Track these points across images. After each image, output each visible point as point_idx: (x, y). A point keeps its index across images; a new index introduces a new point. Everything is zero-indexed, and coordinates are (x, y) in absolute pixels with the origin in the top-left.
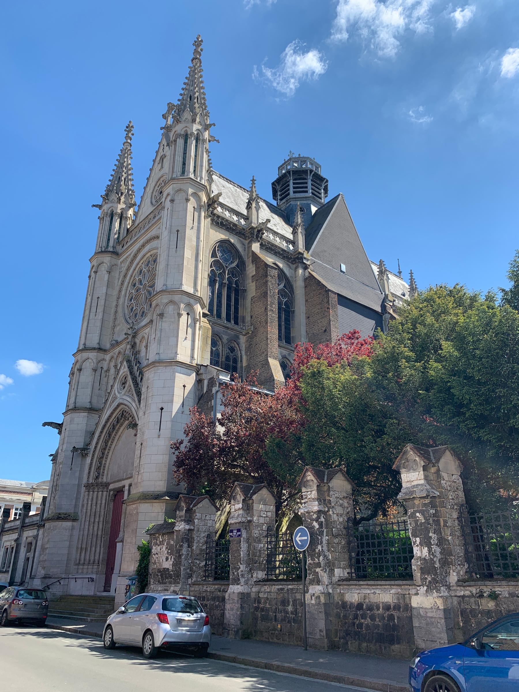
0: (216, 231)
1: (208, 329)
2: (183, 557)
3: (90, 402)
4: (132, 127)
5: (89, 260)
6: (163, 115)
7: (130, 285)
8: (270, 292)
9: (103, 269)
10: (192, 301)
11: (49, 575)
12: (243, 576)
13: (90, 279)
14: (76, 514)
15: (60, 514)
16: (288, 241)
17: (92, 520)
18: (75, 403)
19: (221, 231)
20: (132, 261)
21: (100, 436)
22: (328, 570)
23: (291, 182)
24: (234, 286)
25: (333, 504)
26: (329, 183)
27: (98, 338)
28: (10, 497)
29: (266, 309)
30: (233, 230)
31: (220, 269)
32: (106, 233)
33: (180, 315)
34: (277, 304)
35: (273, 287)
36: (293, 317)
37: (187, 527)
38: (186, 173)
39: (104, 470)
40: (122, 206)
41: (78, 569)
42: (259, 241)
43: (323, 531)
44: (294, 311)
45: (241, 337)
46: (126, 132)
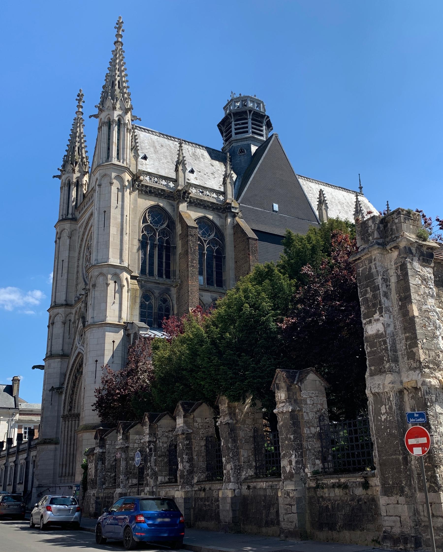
0: (146, 200)
1: (136, 290)
3: (62, 350)
4: (82, 95)
7: (86, 247)
8: (191, 250)
9: (65, 235)
10: (118, 271)
11: (41, 485)
12: (122, 482)
13: (56, 244)
14: (57, 438)
15: (45, 439)
16: (218, 193)
17: (69, 443)
18: (51, 351)
19: (150, 198)
20: (86, 227)
21: (69, 378)
23: (233, 123)
24: (165, 245)
25: (159, 436)
26: (270, 118)
29: (188, 265)
30: (162, 195)
31: (151, 232)
32: (66, 201)
33: (108, 285)
36: (224, 262)
37: (101, 451)
38: (110, 158)
39: (75, 403)
40: (77, 174)
41: (61, 480)
42: (186, 201)
44: (225, 257)
45: (172, 289)
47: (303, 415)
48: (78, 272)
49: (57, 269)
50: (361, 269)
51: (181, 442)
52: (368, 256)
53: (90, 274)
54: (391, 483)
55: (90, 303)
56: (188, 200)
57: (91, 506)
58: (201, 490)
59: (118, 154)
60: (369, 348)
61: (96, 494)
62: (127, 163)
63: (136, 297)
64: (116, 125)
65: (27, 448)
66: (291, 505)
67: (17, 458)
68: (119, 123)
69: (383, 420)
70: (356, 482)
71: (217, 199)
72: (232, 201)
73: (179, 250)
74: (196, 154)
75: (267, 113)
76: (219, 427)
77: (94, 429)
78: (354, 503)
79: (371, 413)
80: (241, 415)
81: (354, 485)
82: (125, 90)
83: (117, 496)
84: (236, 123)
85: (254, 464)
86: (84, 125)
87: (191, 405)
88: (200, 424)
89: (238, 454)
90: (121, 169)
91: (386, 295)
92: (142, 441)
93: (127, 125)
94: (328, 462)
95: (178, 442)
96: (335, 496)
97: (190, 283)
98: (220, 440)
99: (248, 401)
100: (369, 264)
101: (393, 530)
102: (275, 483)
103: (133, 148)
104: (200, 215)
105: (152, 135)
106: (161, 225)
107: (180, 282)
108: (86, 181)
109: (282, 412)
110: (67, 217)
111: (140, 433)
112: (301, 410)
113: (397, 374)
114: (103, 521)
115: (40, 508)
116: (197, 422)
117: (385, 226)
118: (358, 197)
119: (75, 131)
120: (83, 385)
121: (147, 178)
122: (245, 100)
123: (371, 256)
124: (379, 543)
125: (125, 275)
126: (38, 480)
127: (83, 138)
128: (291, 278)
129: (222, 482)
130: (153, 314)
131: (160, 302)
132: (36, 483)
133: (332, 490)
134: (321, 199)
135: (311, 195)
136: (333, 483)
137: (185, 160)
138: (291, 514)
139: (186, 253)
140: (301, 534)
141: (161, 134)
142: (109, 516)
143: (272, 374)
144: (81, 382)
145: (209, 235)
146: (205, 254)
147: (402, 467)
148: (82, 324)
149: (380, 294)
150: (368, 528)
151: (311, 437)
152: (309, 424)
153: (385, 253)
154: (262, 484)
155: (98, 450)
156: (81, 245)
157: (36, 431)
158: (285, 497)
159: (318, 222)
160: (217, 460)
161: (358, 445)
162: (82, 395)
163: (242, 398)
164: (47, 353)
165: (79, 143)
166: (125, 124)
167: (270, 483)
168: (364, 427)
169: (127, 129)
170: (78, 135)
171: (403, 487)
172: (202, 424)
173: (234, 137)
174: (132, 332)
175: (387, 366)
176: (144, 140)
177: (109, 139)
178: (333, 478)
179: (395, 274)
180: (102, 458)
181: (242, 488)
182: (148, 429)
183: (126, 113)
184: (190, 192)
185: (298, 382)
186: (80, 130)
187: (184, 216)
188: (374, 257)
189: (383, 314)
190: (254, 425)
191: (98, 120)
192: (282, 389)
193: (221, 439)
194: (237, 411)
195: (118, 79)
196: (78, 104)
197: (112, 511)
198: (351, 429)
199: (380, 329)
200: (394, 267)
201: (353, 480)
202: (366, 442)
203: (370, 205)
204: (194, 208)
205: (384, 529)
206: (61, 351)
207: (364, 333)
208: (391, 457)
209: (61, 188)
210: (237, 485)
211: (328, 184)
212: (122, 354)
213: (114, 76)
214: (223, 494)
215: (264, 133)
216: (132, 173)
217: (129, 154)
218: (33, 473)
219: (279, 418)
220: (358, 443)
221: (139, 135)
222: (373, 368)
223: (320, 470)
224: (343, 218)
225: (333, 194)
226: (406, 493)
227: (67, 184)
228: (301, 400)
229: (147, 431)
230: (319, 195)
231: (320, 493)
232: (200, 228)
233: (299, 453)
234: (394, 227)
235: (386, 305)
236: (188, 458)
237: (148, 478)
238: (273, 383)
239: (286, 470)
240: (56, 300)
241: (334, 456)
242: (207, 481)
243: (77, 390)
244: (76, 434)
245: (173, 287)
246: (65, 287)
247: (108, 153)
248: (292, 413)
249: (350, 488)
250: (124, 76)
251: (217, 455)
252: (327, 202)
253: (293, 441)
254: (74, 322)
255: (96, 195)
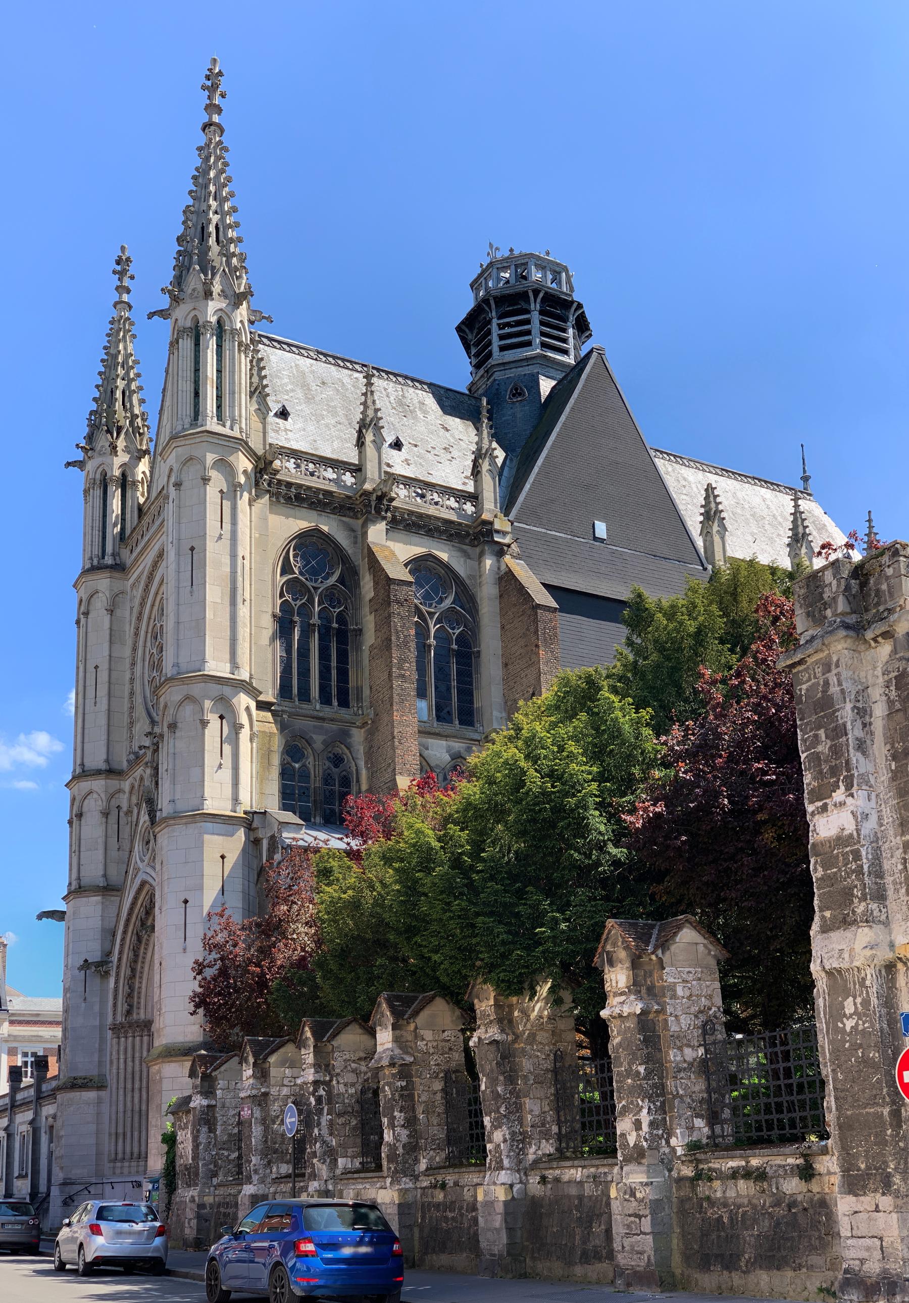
0: (287, 517)
1: (271, 734)
2: (201, 1147)
3: (105, 875)
4: (128, 260)
5: (74, 586)
6: (178, 239)
7: (149, 635)
8: (398, 638)
10: (227, 690)
11: (70, 1179)
12: (256, 1171)
13: (79, 627)
14: (102, 1076)
15: (75, 1079)
16: (462, 496)
17: (129, 1086)
18: (79, 878)
20: (147, 586)
21: (123, 939)
22: (328, 1160)
23: (495, 322)
24: (335, 625)
25: (337, 1071)
27: (104, 750)
28: (52, 1034)
29: (390, 674)
30: (325, 504)
31: (302, 595)
32: (98, 524)
33: (204, 723)
34: (414, 660)
35: (403, 626)
36: (478, 665)
37: (205, 1102)
38: (200, 418)
39: (139, 998)
40: (122, 458)
41: (114, 1168)
42: (384, 518)
43: (322, 1109)
44: (479, 652)
46: (117, 276)
47: (666, 1021)
48: (132, 693)
49: (85, 687)
50: (804, 687)
51: (389, 1084)
52: (821, 655)
53: (162, 699)
54: (863, 1166)
55: (165, 767)
56: (389, 514)
57: (187, 1225)
58: (435, 1187)
59: (219, 407)
60: (820, 869)
61: (197, 1199)
62: (241, 428)
63: (270, 751)
64: (212, 335)
65: (34, 1099)
66: (640, 1217)
67: (11, 1121)
68: (220, 330)
69: (848, 1029)
70: (784, 1166)
71: (459, 511)
72: (496, 516)
73: (370, 638)
74: (408, 401)
75: (576, 297)
76: (476, 1050)
77: (186, 1055)
78: (781, 1211)
79: (822, 1015)
80: (526, 1024)
81: (781, 1172)
82: (232, 248)
83: (247, 1201)
84: (502, 321)
85: (555, 1129)
86: (134, 336)
87: (407, 1002)
88: (430, 1045)
89: (519, 1107)
90: (227, 444)
91: (861, 746)
92: (299, 1081)
93: (239, 334)
94: (722, 1122)
95: (382, 1083)
96: (739, 1195)
97: (396, 716)
98: (475, 1078)
99: (544, 989)
100: (823, 674)
101: (866, 1267)
102: (602, 1170)
103: (256, 389)
104: (417, 550)
105: (298, 357)
106: (326, 578)
107: (372, 716)
108: (144, 473)
109: (620, 1016)
110: (101, 561)
111: (295, 1064)
112: (662, 1009)
113: (882, 926)
114: (221, 1255)
115: (74, 1228)
116: (423, 1039)
117: (863, 585)
118: (800, 502)
119: (112, 351)
120: (156, 956)
121: (291, 464)
122: (523, 264)
123: (829, 655)
124: (834, 1295)
125: (244, 701)
126: (62, 1168)
127: (132, 368)
128: (639, 706)
129: (482, 1168)
130: (312, 791)
131: (327, 763)
132: (58, 1176)
133: (731, 1183)
134: (710, 509)
135: (684, 497)
136: (732, 1168)
137: (381, 418)
138: (638, 1235)
139: (386, 645)
140: (661, 1277)
141: (322, 354)
142: (234, 1243)
143: (596, 933)
144: (150, 949)
145: (441, 600)
146: (430, 646)
147: (889, 1132)
148: (147, 817)
149: (848, 745)
150: (809, 1263)
151: (685, 1069)
152: (680, 1041)
153: (862, 647)
154: (573, 1171)
155: (198, 1102)
156: (137, 629)
157: (52, 1061)
158: (626, 1200)
159: (703, 565)
160: (471, 1123)
161: (792, 1084)
162: (157, 978)
163: (526, 985)
164: (70, 884)
165: (123, 379)
166: (235, 332)
167: (592, 1170)
168: (805, 1045)
169: (240, 344)
170: (120, 359)
171: (889, 1175)
172: (435, 1044)
173: (497, 356)
174: (264, 835)
175: (861, 908)
176: (279, 371)
177: (197, 370)
178: (732, 1158)
179: (884, 698)
180: (207, 1118)
181: (527, 1180)
182: (311, 1055)
183: (237, 305)
184: (393, 495)
185: (656, 948)
186: (125, 348)
187: (380, 557)
188: (835, 659)
189: (854, 790)
190: (554, 1044)
191: (169, 323)
192: (620, 965)
193: (481, 1075)
194: (516, 1014)
195: (215, 219)
196: (119, 283)
197: (241, 1232)
198: (775, 1050)
199: (846, 826)
200: (881, 680)
201: (779, 1161)
202: (809, 1079)
203: (827, 520)
204: (402, 535)
205: (845, 1266)
206: (102, 879)
207: (810, 834)
208: (864, 1111)
209: (86, 492)
210: (518, 1176)
211: (727, 471)
212: (243, 885)
213: (205, 212)
214: (486, 1194)
215: (571, 346)
216: (255, 454)
217: (245, 406)
218: (51, 1154)
219: (614, 1030)
220: (790, 1081)
221: (268, 357)
222: (828, 914)
223: (704, 1141)
224: (764, 560)
225: (739, 494)
226: (895, 1187)
227: (98, 482)
228: (663, 987)
229: (310, 1059)
230: (705, 499)
231: (704, 1191)
232: (419, 583)
233: (658, 1104)
234: (884, 587)
235: (862, 770)
236: (405, 1118)
237: (315, 1161)
238: (600, 950)
239: (627, 1142)
240: (85, 761)
241: (735, 1110)
242: (449, 1167)
243: (142, 968)
244: (144, 1065)
245: (357, 727)
246: (104, 729)
247: (196, 405)
248: (643, 1018)
249: (772, 1178)
250: (228, 213)
251: (470, 1111)
252: (723, 515)
253: (644, 1079)
254: (129, 812)
255: (170, 508)
